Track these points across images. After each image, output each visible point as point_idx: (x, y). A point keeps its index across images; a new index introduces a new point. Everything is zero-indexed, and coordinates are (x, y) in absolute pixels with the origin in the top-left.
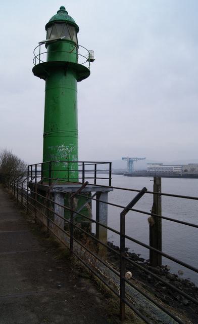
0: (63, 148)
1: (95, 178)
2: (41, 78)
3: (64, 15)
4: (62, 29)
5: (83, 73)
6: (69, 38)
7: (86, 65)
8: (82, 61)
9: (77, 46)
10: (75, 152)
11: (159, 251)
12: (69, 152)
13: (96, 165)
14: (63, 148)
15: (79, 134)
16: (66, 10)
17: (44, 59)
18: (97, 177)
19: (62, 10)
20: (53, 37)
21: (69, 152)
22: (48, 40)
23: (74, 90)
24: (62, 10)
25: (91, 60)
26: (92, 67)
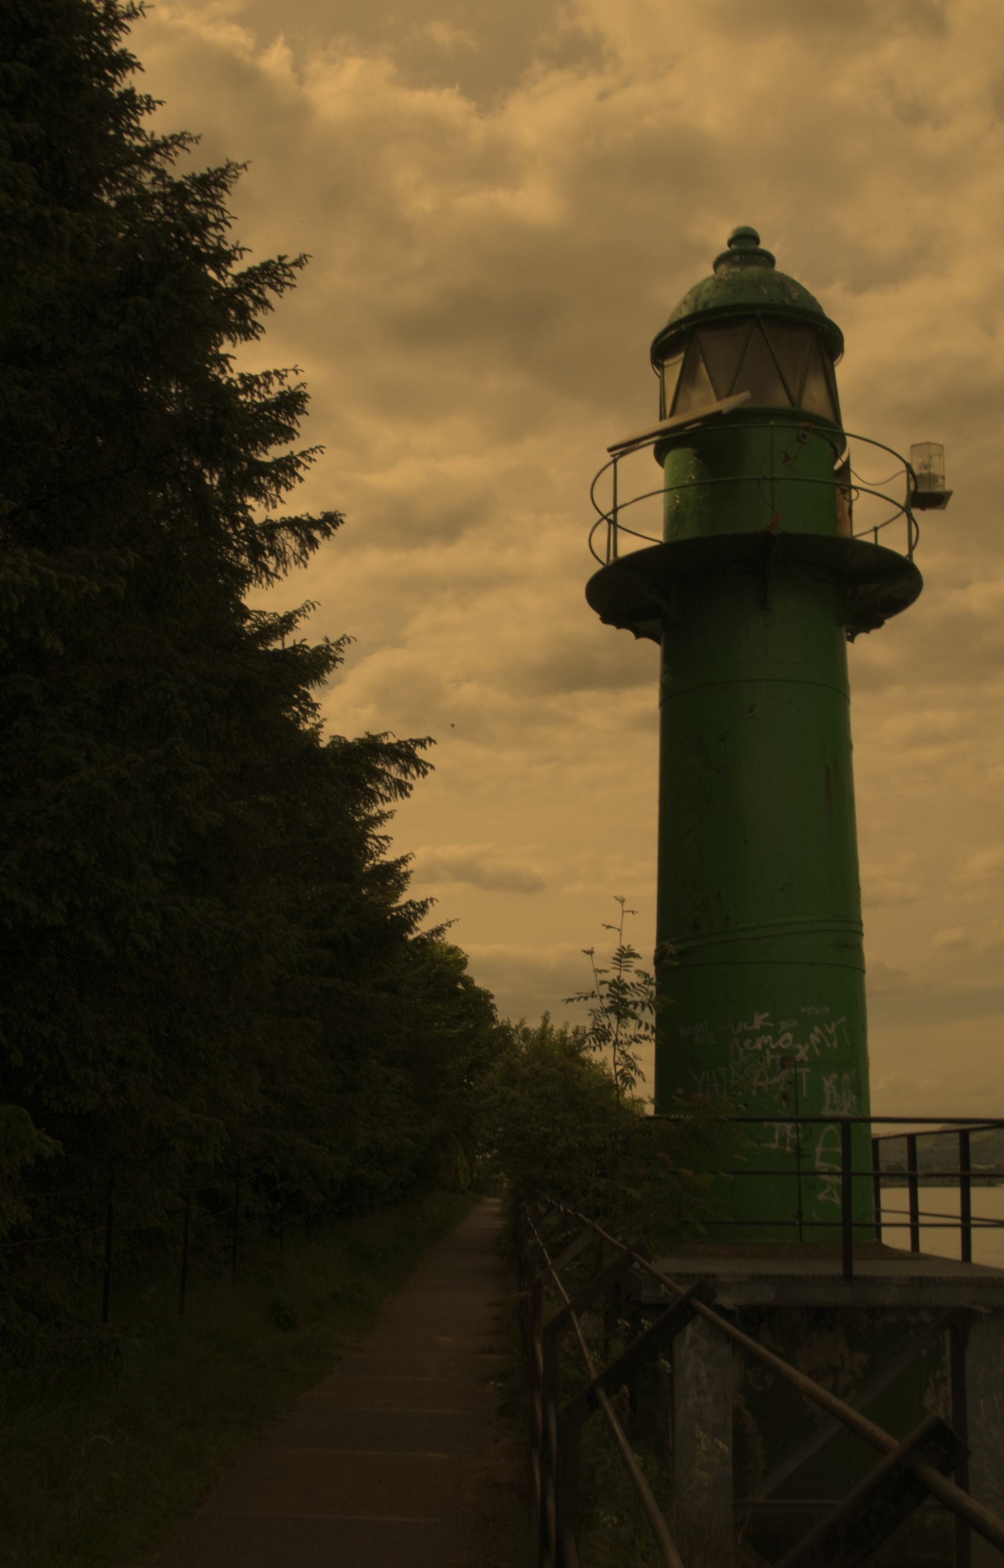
0: (764, 1031)
1: (966, 1222)
2: (638, 635)
3: (754, 271)
4: (547, 1013)
5: (883, 586)
6: (780, 399)
7: (893, 540)
8: (872, 517)
9: (833, 436)
10: (851, 1059)
11: (752, 247)
12: (802, 1054)
13: (964, 1135)
14: (764, 1031)
15: (865, 930)
16: (763, 246)
17: (645, 530)
18: (974, 1212)
19: (745, 246)
20: (705, 402)
21: (802, 1054)
22: (668, 423)
23: (903, 1186)
24: (745, 246)
25: (925, 496)
26: (933, 551)
